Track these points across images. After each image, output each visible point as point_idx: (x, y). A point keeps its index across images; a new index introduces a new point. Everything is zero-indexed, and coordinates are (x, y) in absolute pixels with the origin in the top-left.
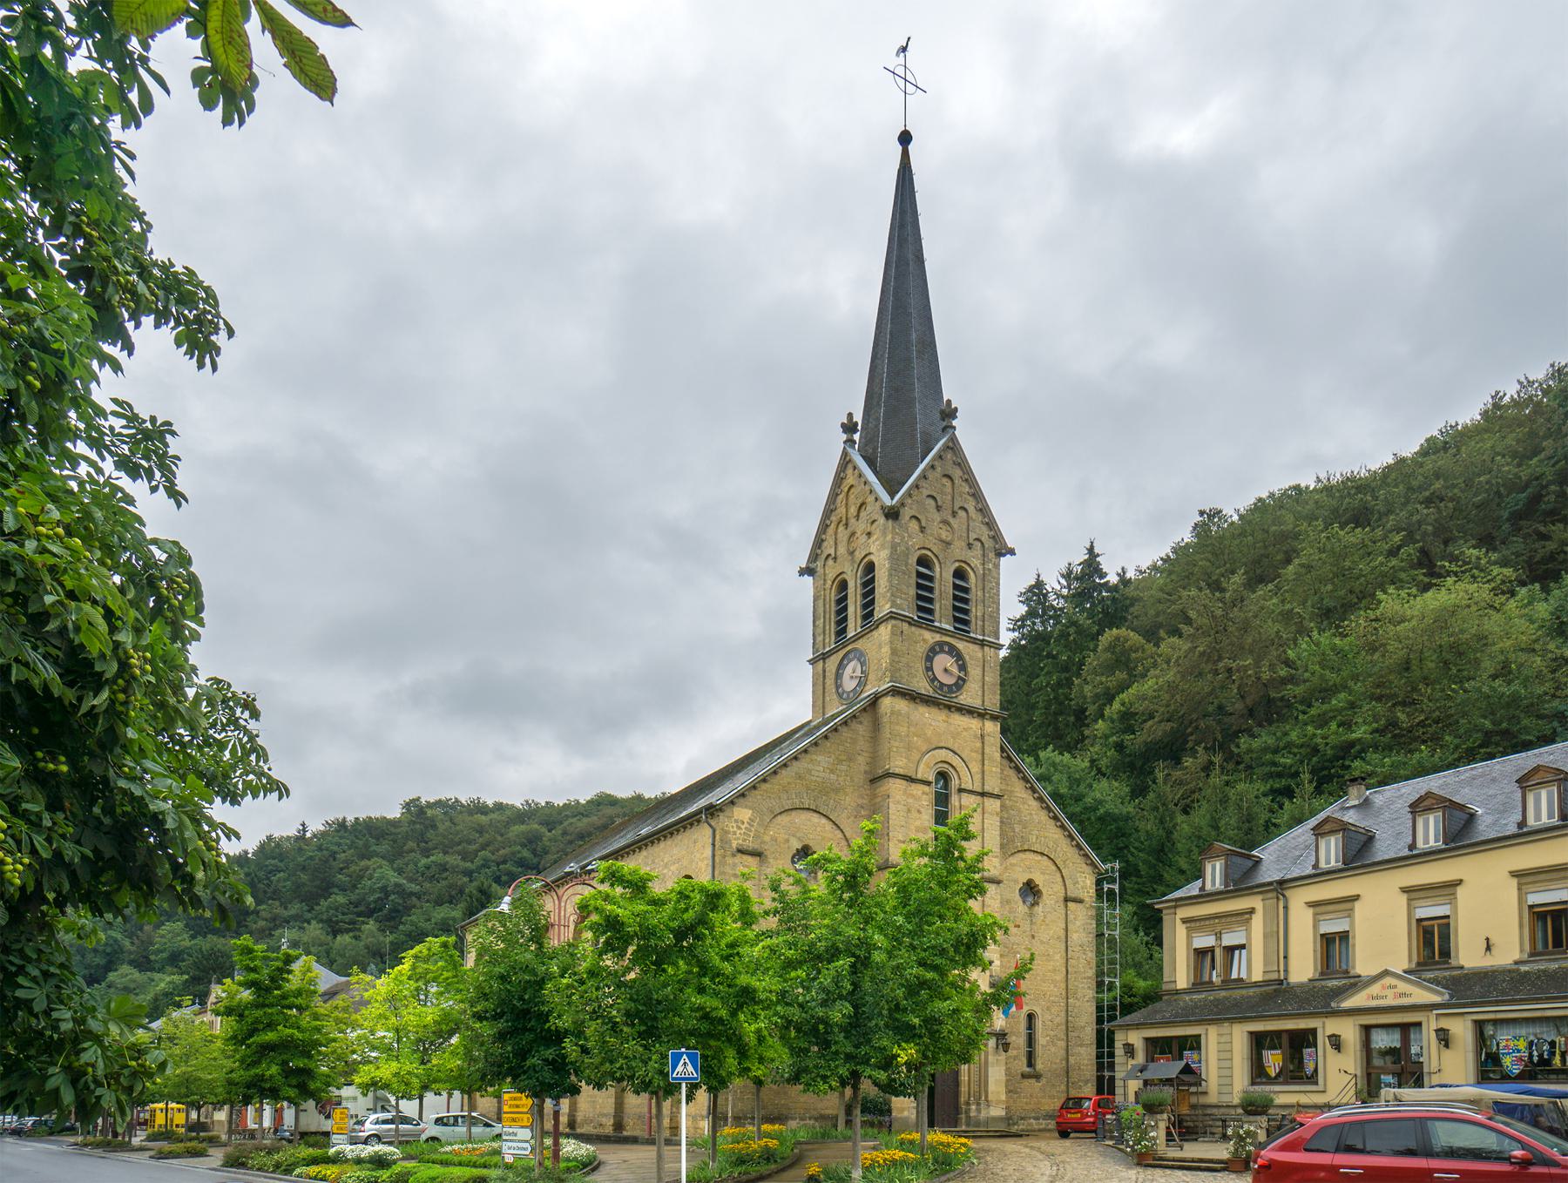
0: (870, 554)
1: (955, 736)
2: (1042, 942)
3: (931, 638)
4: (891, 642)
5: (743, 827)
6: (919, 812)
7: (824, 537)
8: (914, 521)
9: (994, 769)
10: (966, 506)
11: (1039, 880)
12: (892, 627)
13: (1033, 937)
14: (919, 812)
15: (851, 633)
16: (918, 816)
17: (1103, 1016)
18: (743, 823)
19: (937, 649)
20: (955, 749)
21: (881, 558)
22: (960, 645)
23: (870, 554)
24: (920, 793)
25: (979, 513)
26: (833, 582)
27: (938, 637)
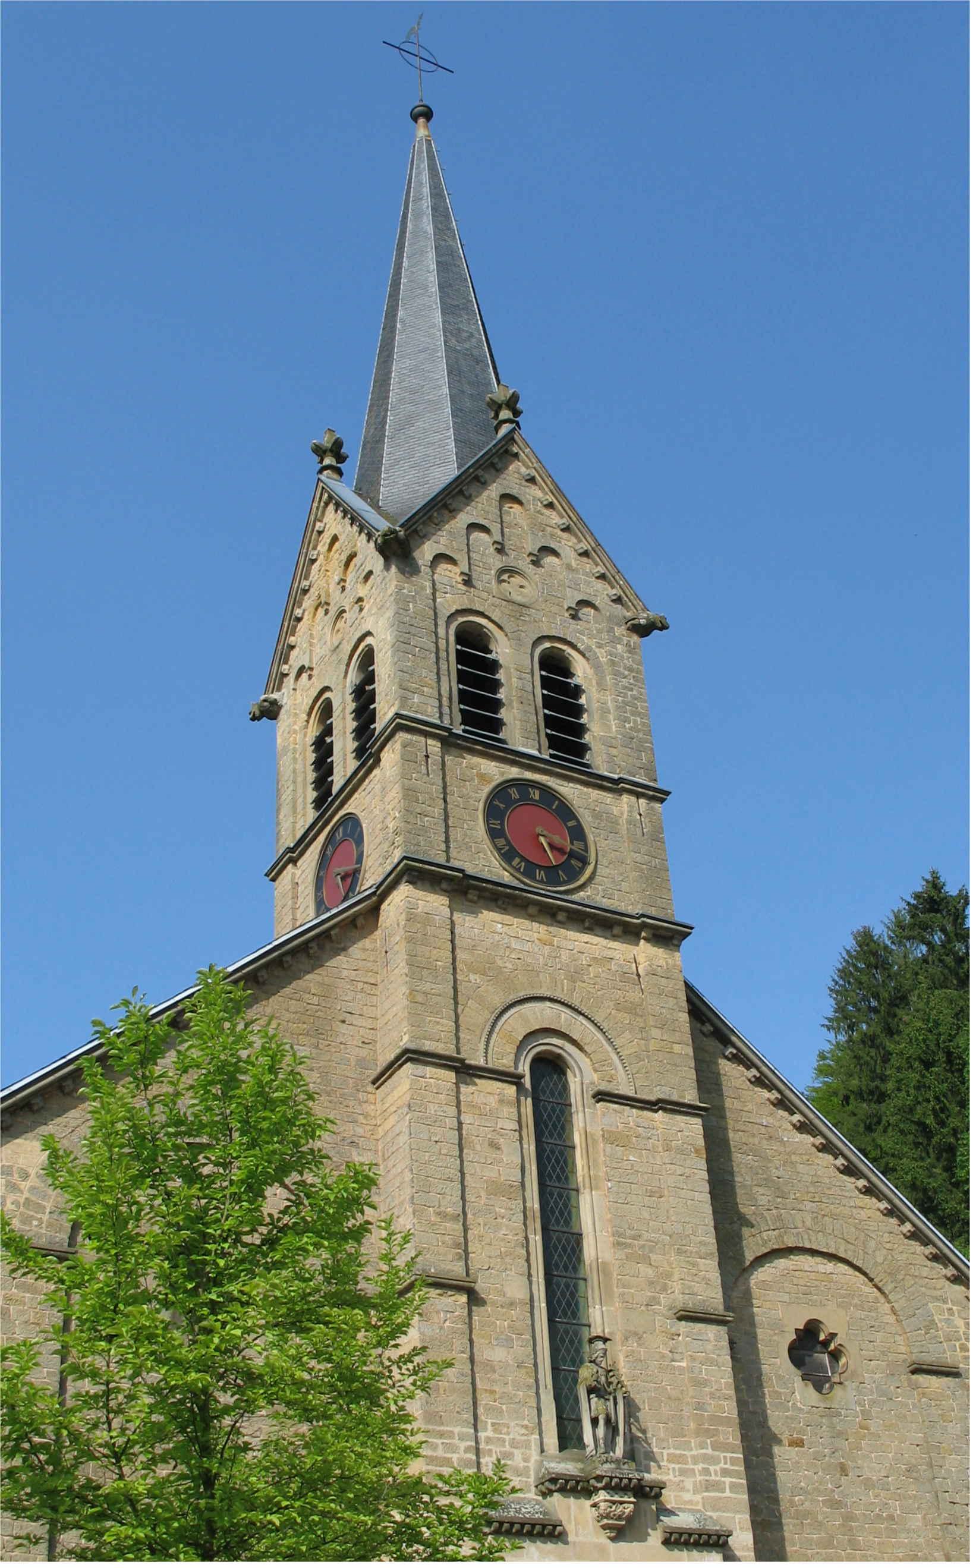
0: (368, 634)
1: (576, 975)
2: (868, 1484)
3: (496, 772)
4: (403, 776)
5: (25, 1185)
6: (495, 1146)
7: (292, 640)
8: (443, 567)
9: (677, 1048)
10: (553, 545)
11: (833, 1322)
12: (405, 746)
13: (843, 1470)
14: (495, 1146)
15: (338, 780)
16: (494, 1155)
17: (731, 1458)
18: (25, 1176)
19: (514, 793)
20: (576, 1003)
21: (383, 642)
22: (569, 791)
23: (368, 634)
24: (493, 1101)
25: (585, 559)
26: (309, 714)
27: (514, 772)
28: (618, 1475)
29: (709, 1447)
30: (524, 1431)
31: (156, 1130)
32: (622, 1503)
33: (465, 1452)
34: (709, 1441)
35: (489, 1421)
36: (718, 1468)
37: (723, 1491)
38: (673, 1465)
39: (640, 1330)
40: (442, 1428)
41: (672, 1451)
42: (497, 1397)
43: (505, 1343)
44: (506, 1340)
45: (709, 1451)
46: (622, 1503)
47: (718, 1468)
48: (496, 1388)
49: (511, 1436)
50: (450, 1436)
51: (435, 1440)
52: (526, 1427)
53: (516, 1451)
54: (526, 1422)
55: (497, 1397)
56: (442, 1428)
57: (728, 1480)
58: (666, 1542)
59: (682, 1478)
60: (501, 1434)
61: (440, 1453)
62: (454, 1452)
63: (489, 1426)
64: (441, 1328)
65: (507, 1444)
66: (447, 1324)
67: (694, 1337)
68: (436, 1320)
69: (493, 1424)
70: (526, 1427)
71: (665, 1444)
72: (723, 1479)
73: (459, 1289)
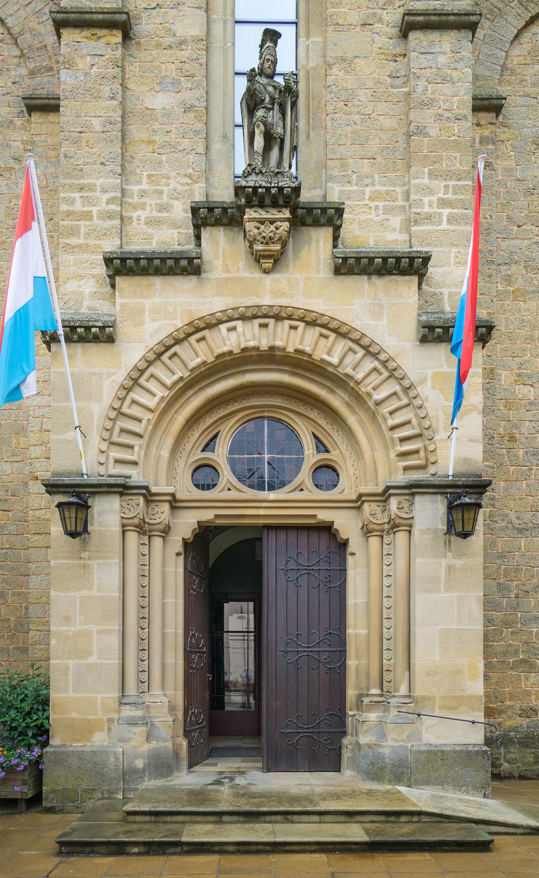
28: (264, 184)
29: (426, 175)
30: (187, 180)
31: (161, 184)
32: (272, 222)
33: (108, 203)
34: (426, 170)
35: (145, 173)
36: (434, 199)
37: (440, 223)
38: (376, 203)
39: (350, 55)
40: (82, 181)
41: (377, 187)
42: (156, 147)
43: (171, 88)
44: (173, 84)
45: (426, 181)
46: (272, 222)
47: (434, 199)
48: (156, 138)
49: (172, 187)
50: (91, 188)
51: (72, 195)
52: (190, 176)
53: (176, 203)
54: (190, 171)
55: (156, 147)
56: (82, 181)
57: (446, 212)
58: (338, 271)
59: (386, 217)
60: (159, 185)
61: (78, 207)
62: (93, 206)
63: (145, 180)
64: (86, 74)
65: (165, 195)
66: (95, 69)
67: (423, 50)
68: (81, 66)
69: (149, 177)
70: (190, 176)
71: (367, 181)
72: (439, 211)
73: (110, 25)
